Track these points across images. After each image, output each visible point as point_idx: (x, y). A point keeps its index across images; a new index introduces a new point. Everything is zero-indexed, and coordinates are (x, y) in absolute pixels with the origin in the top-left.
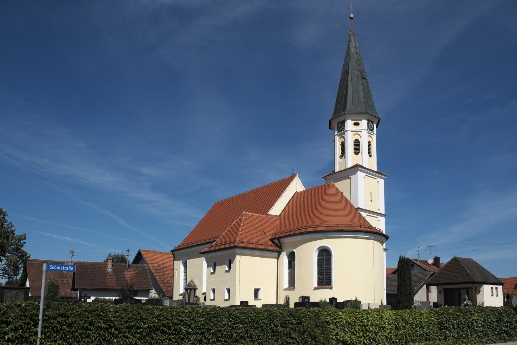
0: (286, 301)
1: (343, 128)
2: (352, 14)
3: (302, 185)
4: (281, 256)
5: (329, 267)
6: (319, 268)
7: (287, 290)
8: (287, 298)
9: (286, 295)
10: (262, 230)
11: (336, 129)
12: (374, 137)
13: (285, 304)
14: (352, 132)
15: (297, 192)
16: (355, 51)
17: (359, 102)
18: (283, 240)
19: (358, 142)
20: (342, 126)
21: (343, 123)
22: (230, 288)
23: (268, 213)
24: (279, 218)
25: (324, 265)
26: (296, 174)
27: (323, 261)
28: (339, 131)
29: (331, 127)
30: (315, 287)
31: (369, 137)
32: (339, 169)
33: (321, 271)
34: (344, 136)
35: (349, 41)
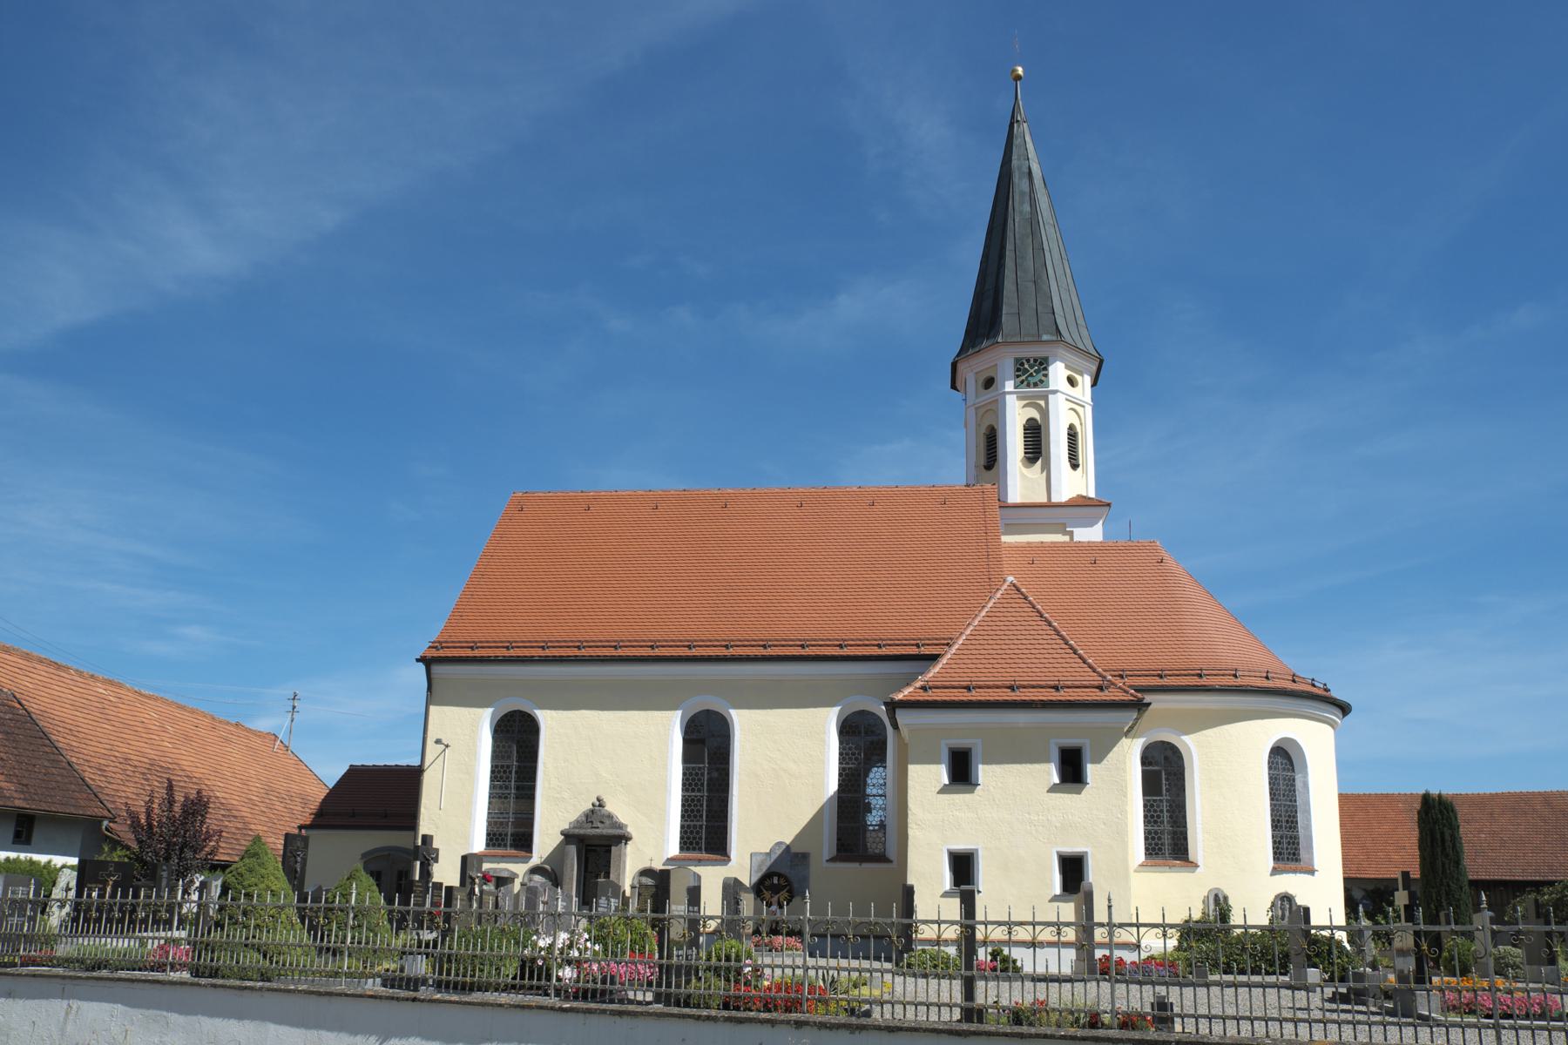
14: (1067, 400)
21: (1043, 364)
22: (1086, 853)
29: (958, 385)
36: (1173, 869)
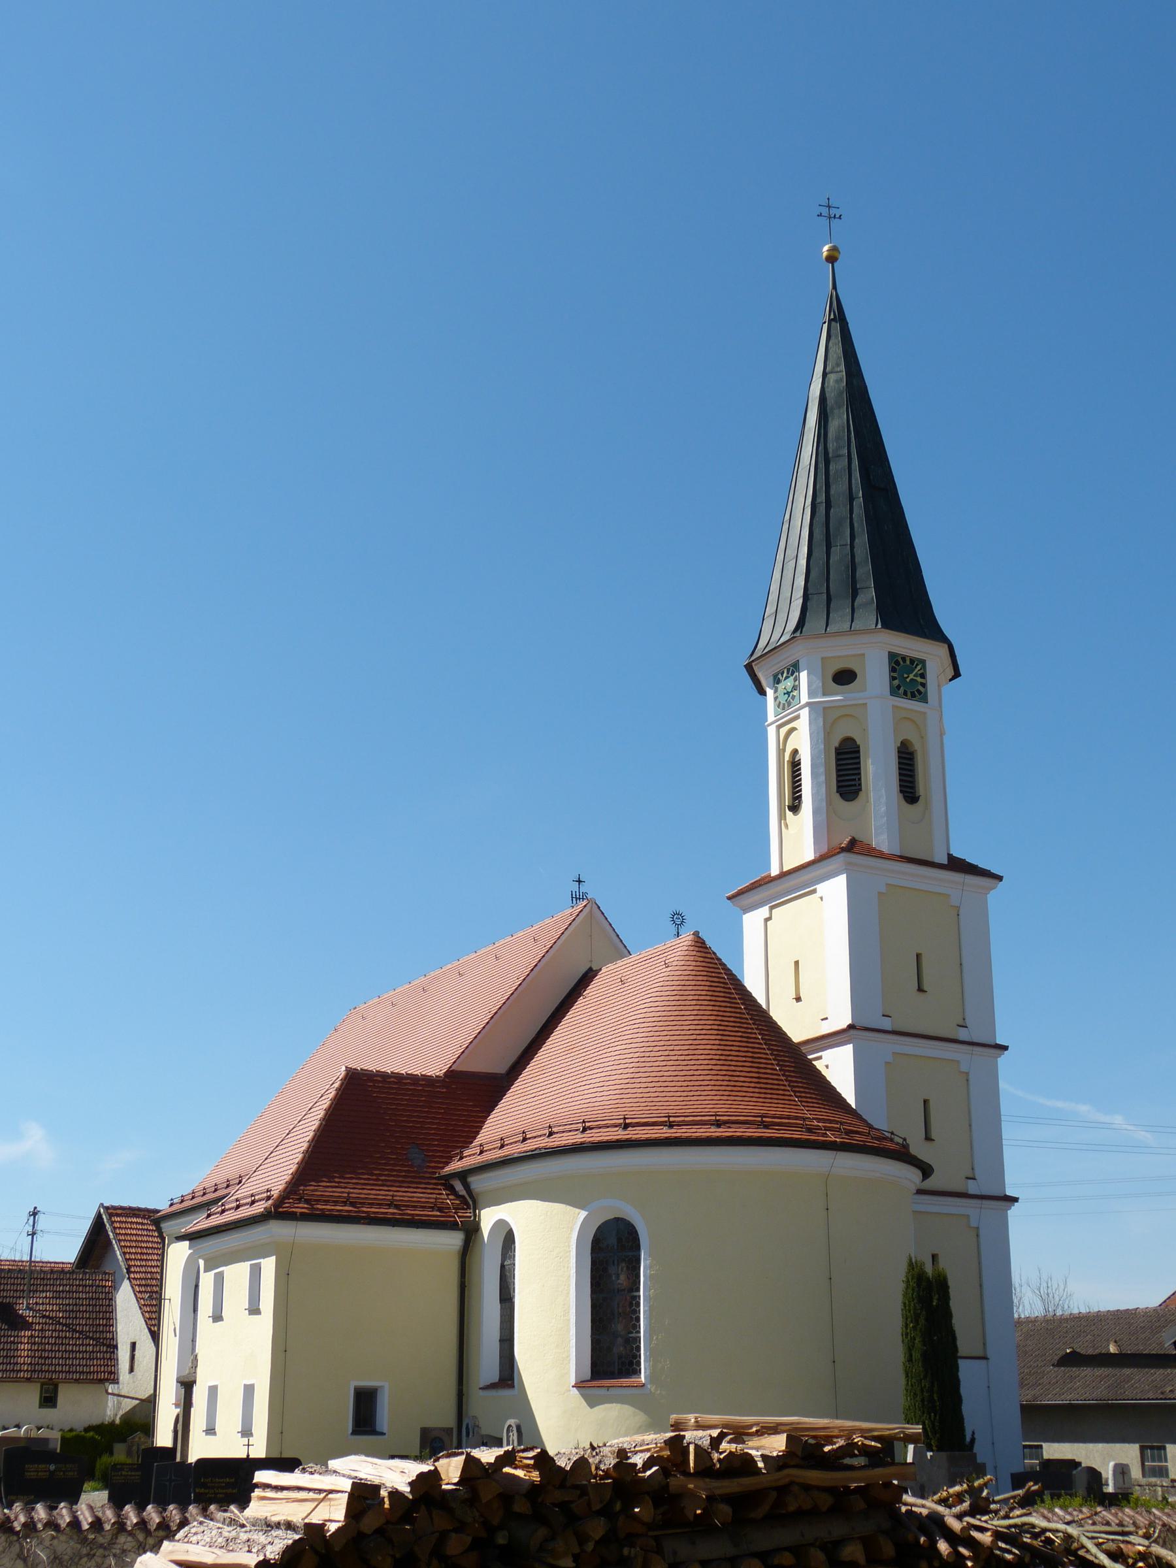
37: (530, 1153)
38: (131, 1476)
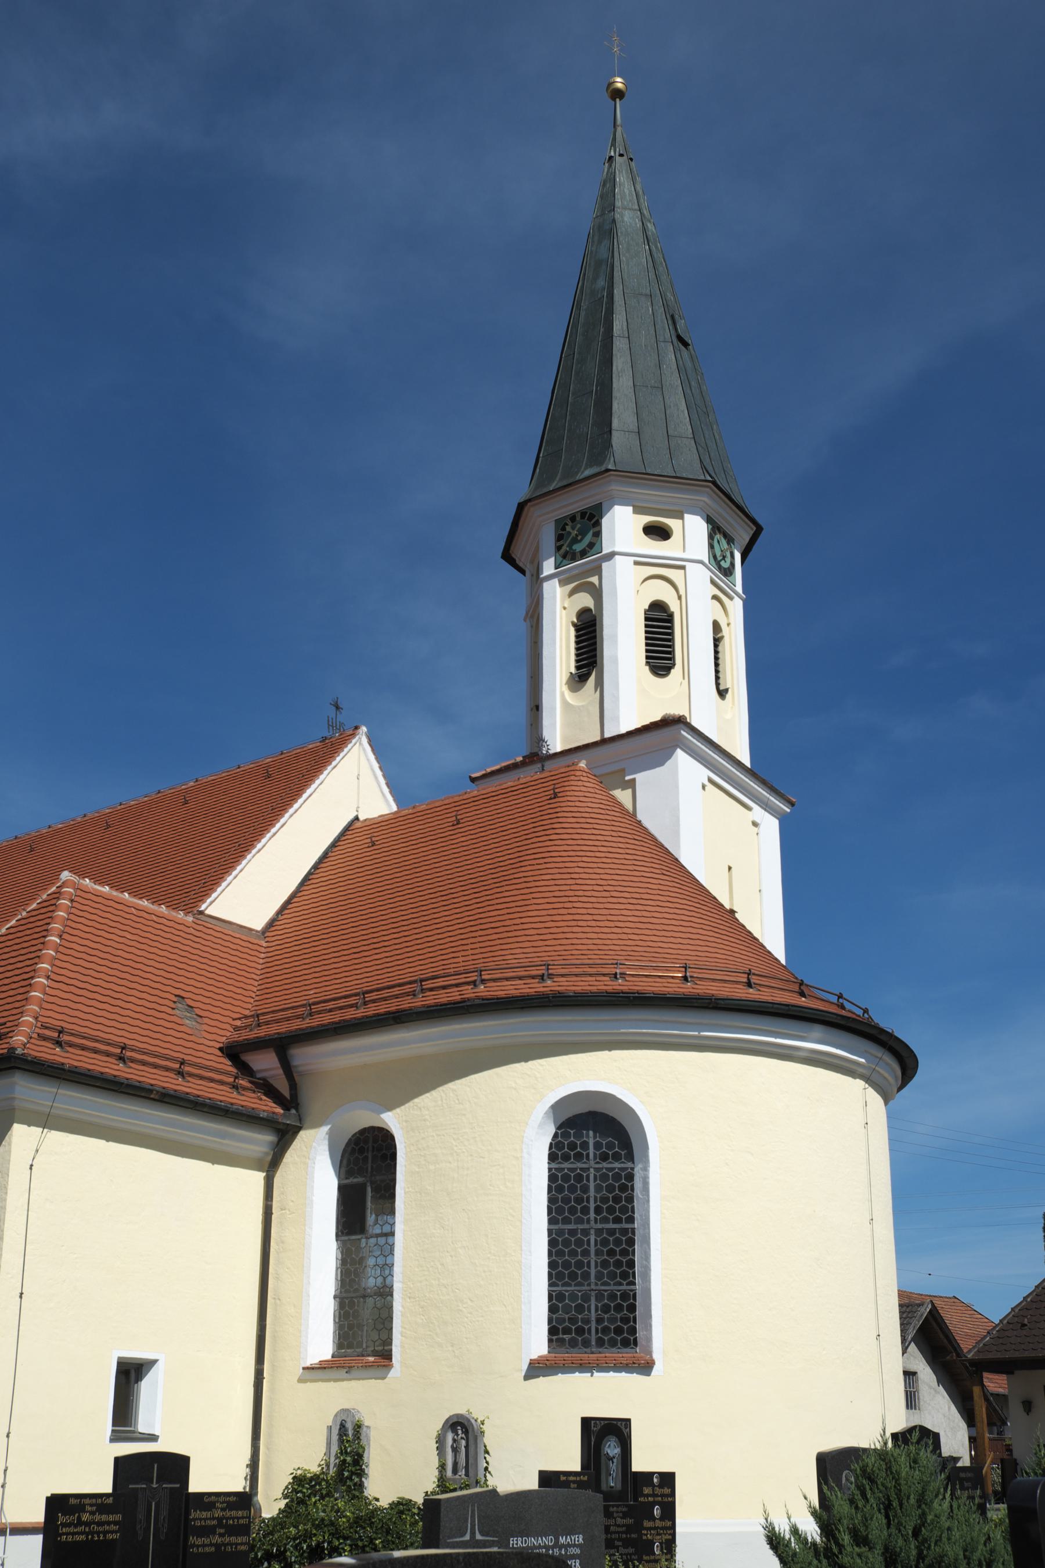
0: (343, 1452)
1: (591, 545)
2: (619, 76)
3: (386, 790)
4: (291, 1156)
5: (624, 1232)
6: (560, 1232)
7: (328, 1374)
8: (349, 1426)
9: (345, 1411)
10: (178, 992)
11: (553, 549)
12: (736, 607)
13: (332, 1471)
14: (636, 563)
15: (357, 818)
16: (639, 225)
17: (670, 432)
18: (304, 1056)
19: (663, 616)
20: (583, 533)
23: (203, 908)
24: (265, 945)
25: (592, 1215)
26: (357, 728)
27: (585, 1189)
28: (566, 554)
30: (535, 1356)
31: (715, 602)
32: (565, 739)
33: (574, 1253)
34: (594, 580)
35: (610, 182)
36: (355, 1373)
37: (435, 1008)
38: (100, 1524)
